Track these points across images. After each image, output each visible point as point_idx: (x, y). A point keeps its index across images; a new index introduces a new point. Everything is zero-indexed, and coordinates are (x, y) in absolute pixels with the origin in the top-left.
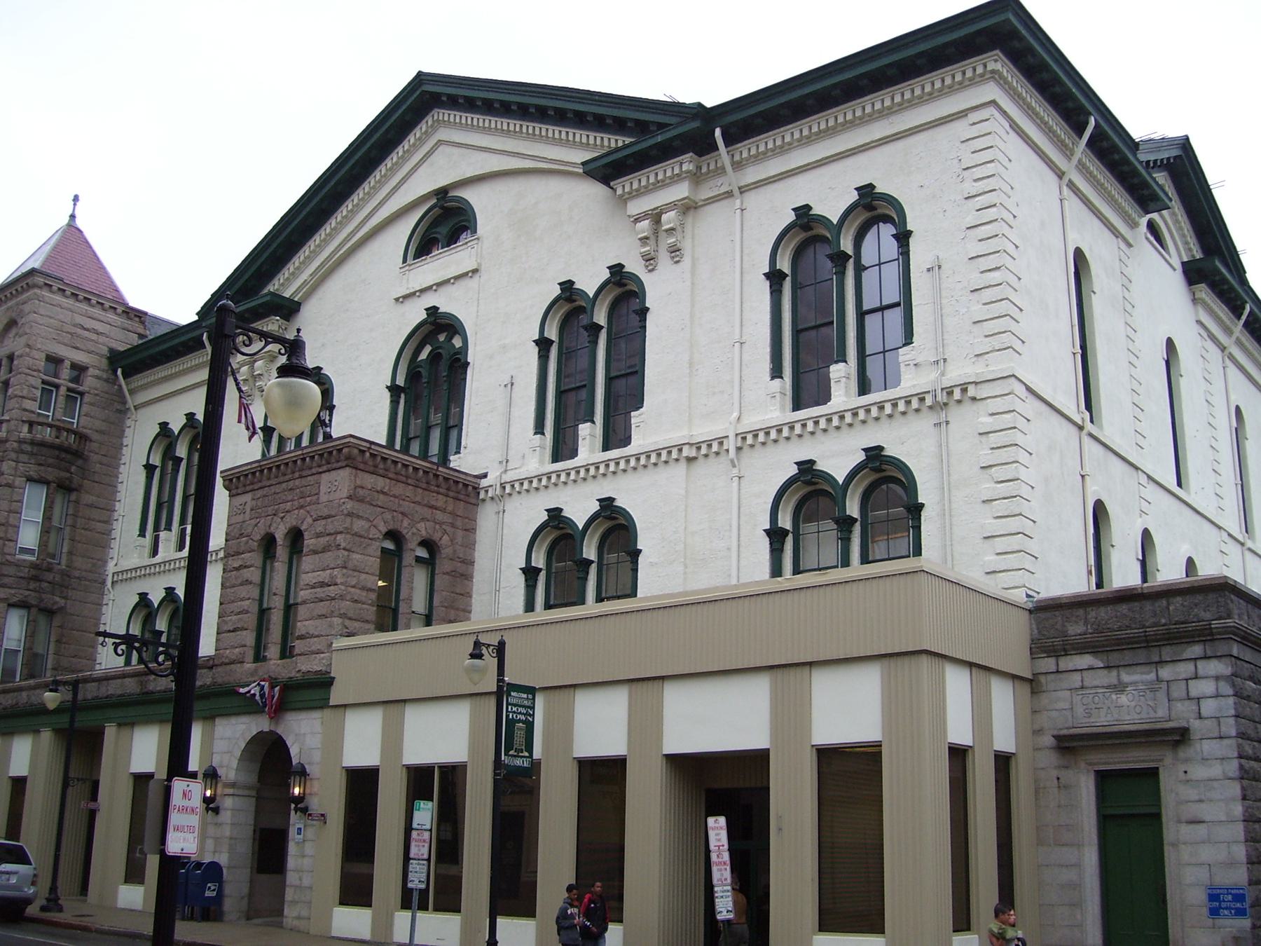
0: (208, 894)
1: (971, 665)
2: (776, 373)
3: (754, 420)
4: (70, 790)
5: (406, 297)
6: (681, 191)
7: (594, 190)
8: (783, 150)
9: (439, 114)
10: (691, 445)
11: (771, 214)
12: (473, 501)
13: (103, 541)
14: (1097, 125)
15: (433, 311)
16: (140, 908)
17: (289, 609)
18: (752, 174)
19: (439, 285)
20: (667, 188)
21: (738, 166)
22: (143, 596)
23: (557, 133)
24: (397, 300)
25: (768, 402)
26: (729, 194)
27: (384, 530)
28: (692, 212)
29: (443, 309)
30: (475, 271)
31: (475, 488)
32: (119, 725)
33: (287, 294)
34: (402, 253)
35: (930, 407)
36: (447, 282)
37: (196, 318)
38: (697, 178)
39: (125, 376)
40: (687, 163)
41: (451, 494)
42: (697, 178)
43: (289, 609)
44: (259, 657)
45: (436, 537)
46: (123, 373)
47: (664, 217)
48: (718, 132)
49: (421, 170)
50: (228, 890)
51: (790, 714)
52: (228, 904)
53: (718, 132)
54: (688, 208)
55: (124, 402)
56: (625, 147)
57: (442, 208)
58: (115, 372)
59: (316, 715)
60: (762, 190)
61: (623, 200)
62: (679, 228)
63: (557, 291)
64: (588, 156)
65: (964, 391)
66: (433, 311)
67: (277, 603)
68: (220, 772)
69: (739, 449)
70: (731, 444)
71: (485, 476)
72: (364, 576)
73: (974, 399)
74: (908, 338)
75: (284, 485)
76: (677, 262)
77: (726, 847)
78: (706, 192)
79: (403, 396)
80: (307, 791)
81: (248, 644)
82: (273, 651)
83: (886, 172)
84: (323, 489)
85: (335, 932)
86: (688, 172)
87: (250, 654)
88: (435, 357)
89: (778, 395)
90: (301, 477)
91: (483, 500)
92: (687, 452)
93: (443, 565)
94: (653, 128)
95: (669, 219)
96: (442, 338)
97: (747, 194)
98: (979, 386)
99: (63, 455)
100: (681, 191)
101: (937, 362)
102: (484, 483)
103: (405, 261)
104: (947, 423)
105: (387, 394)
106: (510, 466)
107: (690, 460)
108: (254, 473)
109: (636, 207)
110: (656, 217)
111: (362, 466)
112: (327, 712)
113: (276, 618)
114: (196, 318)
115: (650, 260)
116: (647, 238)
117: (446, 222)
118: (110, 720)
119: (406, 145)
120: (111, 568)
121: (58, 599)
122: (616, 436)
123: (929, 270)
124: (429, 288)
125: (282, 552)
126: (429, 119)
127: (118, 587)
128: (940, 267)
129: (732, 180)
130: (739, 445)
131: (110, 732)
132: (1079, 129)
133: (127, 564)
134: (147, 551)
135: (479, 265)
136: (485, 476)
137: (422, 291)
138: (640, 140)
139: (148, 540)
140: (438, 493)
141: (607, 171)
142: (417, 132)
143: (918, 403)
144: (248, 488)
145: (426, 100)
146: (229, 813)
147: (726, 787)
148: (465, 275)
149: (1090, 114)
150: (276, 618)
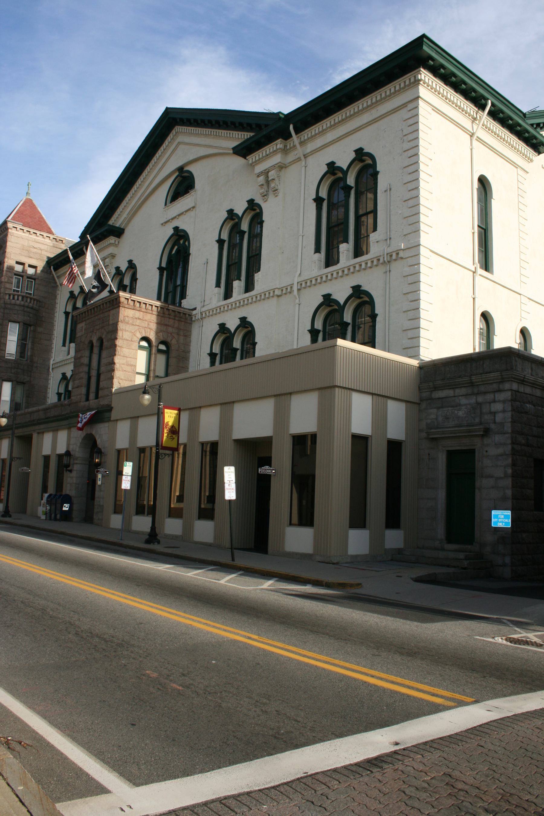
0: (64, 509)
1: (372, 394)
2: (318, 250)
3: (306, 276)
4: (13, 463)
5: (166, 223)
6: (277, 159)
7: (239, 161)
8: (323, 132)
9: (178, 129)
10: (279, 289)
11: (317, 168)
12: (189, 322)
13: (48, 350)
14: (493, 105)
15: (176, 229)
16: (120, 527)
17: (99, 376)
18: (310, 147)
19: (179, 215)
20: (271, 156)
21: (302, 143)
22: (64, 374)
23: (237, 135)
24: (162, 224)
25: (312, 263)
26: (299, 159)
27: (140, 337)
28: (283, 170)
29: (181, 228)
30: (194, 207)
31: (189, 315)
32: (38, 433)
33: (117, 226)
34: (164, 201)
35: (382, 264)
36: (182, 214)
37: (79, 240)
38: (285, 151)
39: (55, 269)
40: (279, 144)
41: (177, 319)
42: (285, 151)
43: (99, 376)
44: (87, 399)
45: (169, 340)
46: (54, 269)
47: (270, 174)
48: (291, 127)
49: (172, 159)
50: (75, 507)
51: (281, 417)
52: (75, 514)
53: (291, 127)
54: (281, 167)
55: (56, 283)
56: (251, 138)
57: (182, 177)
58: (50, 268)
59: (106, 424)
60: (314, 155)
61: (252, 166)
62: (277, 179)
63: (226, 215)
64: (235, 144)
65: (398, 254)
66: (176, 229)
67: (94, 373)
68: (72, 453)
69: (299, 290)
70: (295, 288)
71: (195, 309)
72: (129, 359)
73: (402, 258)
74: (375, 229)
75: (97, 317)
76: (276, 196)
77: (234, 481)
78: (291, 157)
79: (165, 272)
80: (103, 460)
81: (83, 393)
82: (92, 396)
83: (366, 141)
84: (111, 318)
85: (112, 526)
86: (280, 149)
87: (84, 398)
88: (178, 251)
89: (317, 261)
90: (103, 313)
91: (194, 321)
92: (277, 292)
93: (173, 354)
94: (263, 127)
95: (272, 174)
96: (182, 242)
97: (309, 158)
98: (405, 251)
99: (26, 309)
100: (277, 159)
101: (386, 240)
102: (194, 312)
103: (166, 204)
104: (390, 271)
105: (158, 272)
106: (206, 303)
107: (278, 296)
108: (85, 312)
109: (259, 168)
110: (266, 173)
111: (127, 306)
112: (110, 423)
113: (93, 380)
114: (79, 240)
115: (265, 196)
116: (262, 185)
117: (183, 184)
118: (34, 431)
119: (164, 145)
120: (52, 362)
121: (26, 377)
122: (249, 287)
123: (385, 191)
124: (175, 218)
125: (96, 350)
126: (174, 132)
127: (55, 370)
128: (390, 189)
129: (299, 151)
130: (299, 287)
131: (35, 436)
132: (482, 107)
133: (58, 360)
134: (66, 353)
135: (196, 204)
136: (195, 309)
137: (173, 219)
138: (258, 132)
139: (66, 349)
140: (170, 318)
141: (244, 151)
142: (169, 139)
143: (378, 262)
144: (84, 320)
145: (172, 121)
146: (75, 472)
147: (254, 454)
148: (189, 210)
149: (488, 99)
150: (93, 380)
